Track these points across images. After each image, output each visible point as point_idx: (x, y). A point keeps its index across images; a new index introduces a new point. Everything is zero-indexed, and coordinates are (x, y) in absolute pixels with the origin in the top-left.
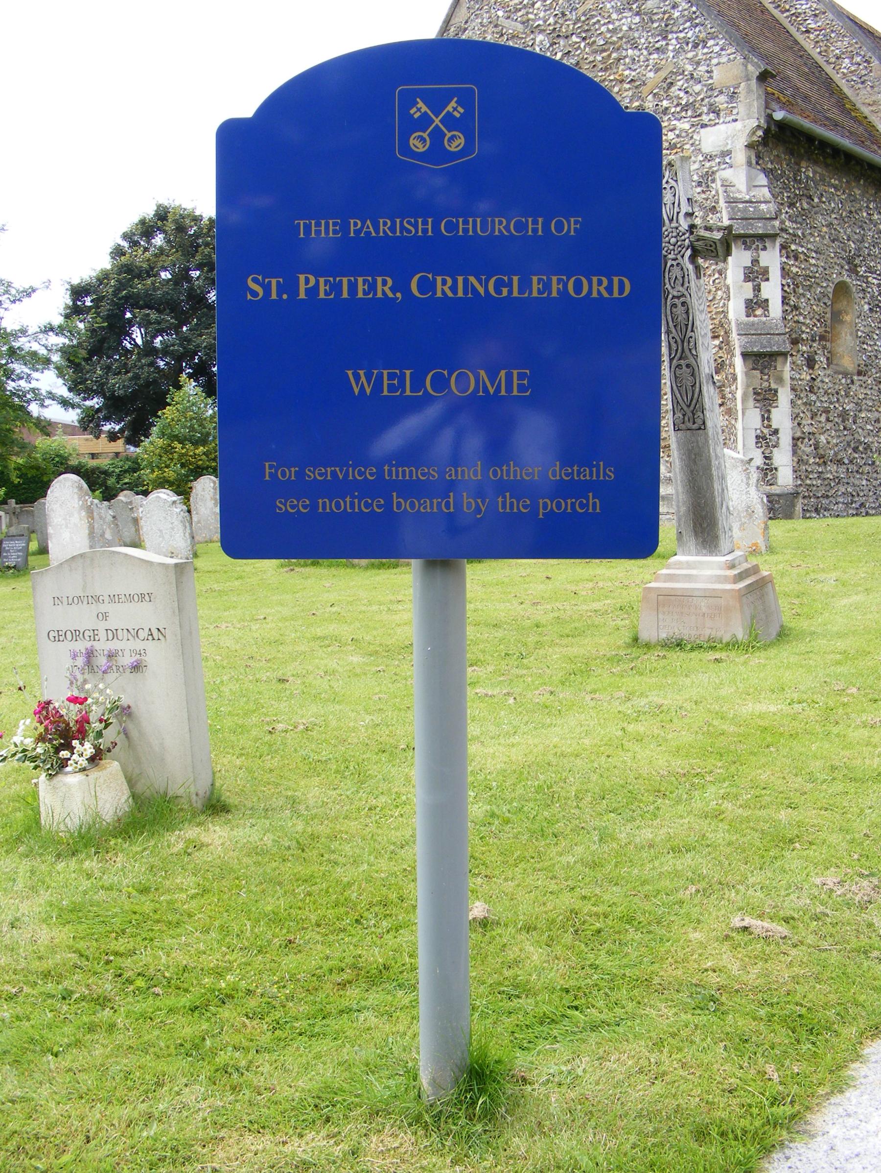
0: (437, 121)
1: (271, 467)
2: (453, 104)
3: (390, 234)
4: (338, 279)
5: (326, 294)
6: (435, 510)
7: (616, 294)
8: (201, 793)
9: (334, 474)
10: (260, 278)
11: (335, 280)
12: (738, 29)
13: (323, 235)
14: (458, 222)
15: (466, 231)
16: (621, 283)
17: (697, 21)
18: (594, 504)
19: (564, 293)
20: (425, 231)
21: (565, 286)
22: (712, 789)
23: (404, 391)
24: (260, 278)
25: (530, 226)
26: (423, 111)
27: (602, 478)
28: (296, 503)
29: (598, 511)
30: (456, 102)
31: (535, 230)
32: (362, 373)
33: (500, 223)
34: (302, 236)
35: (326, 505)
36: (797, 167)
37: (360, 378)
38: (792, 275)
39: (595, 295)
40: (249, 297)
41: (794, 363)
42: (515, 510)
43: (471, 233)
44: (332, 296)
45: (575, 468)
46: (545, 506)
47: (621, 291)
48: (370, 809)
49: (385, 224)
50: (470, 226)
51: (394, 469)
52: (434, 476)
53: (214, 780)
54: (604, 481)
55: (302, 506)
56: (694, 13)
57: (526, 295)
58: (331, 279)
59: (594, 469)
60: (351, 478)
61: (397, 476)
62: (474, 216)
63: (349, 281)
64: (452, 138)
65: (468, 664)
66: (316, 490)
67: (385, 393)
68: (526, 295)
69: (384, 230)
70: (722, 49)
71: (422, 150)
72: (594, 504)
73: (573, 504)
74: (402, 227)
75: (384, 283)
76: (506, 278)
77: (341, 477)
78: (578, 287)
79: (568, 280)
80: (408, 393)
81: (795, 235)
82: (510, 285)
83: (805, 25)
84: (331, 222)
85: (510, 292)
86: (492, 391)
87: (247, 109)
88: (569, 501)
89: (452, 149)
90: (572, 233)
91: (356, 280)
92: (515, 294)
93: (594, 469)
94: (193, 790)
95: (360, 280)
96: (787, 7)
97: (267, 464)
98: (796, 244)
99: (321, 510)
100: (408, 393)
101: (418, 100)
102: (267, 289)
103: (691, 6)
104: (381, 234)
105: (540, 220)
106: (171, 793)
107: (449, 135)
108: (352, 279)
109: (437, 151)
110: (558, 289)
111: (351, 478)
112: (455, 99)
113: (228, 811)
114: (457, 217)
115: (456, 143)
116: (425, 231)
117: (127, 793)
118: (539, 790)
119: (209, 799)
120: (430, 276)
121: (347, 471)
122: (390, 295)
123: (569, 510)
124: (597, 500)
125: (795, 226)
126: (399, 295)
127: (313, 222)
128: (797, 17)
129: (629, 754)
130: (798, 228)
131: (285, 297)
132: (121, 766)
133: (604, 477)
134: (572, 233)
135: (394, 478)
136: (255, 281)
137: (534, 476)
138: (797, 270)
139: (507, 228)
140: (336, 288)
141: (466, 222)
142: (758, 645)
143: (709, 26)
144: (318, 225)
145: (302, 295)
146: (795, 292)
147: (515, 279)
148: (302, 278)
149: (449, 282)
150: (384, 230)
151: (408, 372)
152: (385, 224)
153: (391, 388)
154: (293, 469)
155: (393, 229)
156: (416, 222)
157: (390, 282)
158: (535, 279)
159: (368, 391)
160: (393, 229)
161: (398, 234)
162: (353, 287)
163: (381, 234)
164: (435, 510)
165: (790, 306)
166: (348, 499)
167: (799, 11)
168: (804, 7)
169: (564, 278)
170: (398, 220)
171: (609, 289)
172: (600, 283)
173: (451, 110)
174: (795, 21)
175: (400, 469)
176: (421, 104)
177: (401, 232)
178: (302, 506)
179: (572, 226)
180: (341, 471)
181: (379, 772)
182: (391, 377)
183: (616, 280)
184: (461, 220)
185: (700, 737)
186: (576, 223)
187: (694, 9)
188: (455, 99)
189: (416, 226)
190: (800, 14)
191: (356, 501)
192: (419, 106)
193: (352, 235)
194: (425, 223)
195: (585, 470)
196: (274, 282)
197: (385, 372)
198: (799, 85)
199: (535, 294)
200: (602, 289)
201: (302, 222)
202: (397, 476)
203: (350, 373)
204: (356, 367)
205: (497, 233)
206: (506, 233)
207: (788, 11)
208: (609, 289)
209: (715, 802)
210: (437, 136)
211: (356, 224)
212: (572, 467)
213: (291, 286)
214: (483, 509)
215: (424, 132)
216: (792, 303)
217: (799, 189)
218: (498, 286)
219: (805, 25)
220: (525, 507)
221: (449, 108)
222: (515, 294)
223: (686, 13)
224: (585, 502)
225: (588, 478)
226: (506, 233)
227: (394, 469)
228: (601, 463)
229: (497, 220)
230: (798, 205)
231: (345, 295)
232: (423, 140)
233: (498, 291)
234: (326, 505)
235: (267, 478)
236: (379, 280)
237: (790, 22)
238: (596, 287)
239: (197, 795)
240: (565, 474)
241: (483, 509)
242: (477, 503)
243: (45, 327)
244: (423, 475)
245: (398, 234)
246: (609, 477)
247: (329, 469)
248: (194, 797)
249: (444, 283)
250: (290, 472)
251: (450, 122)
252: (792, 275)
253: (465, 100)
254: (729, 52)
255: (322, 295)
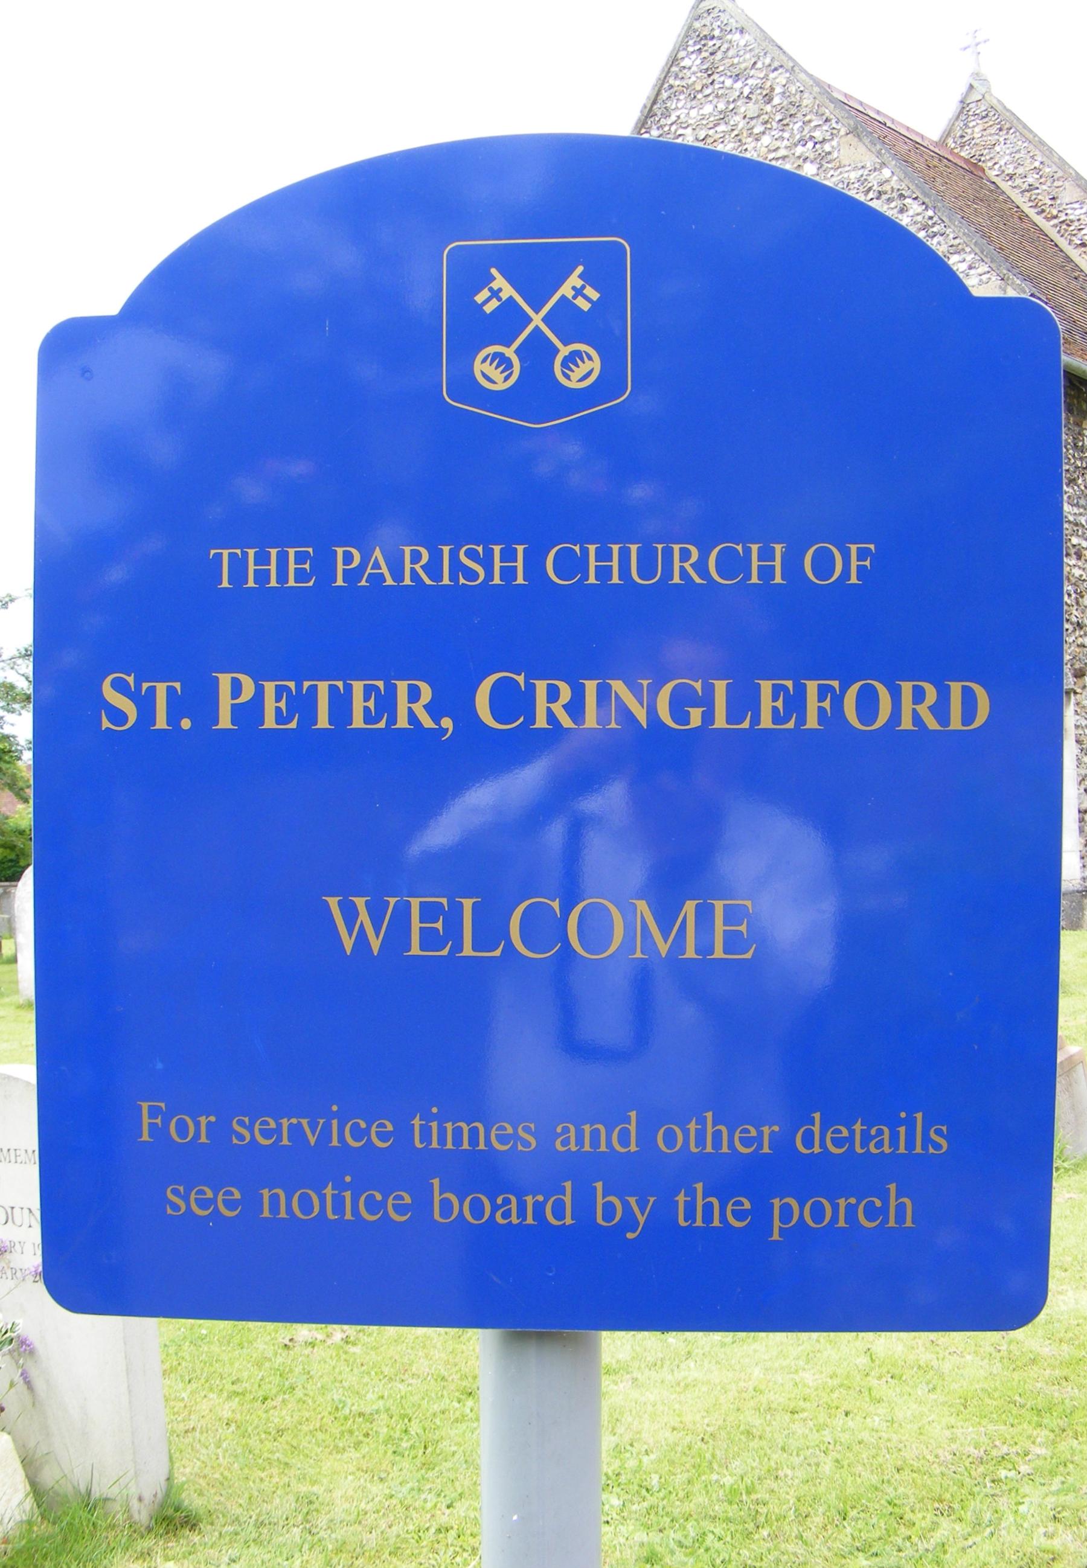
0: (537, 320)
1: (154, 1112)
2: (574, 280)
3: (428, 581)
4: (306, 684)
5: (280, 717)
6: (530, 1220)
7: (956, 723)
8: (148, 1496)
9: (296, 1131)
10: (131, 680)
11: (299, 687)
12: (990, 242)
13: (273, 583)
14: (585, 552)
15: (604, 573)
16: (969, 697)
17: (935, 229)
18: (901, 1208)
19: (834, 718)
20: (508, 574)
21: (838, 702)
22: (1033, 1494)
23: (458, 946)
24: (131, 680)
25: (755, 563)
26: (504, 296)
27: (918, 1150)
28: (210, 1194)
29: (909, 1223)
30: (580, 277)
31: (766, 573)
32: (360, 902)
33: (685, 555)
34: (225, 584)
35: (278, 1203)
36: (1077, 429)
37: (357, 914)
38: (1073, 580)
39: (907, 724)
40: (106, 724)
41: (1078, 704)
42: (716, 1223)
43: (615, 580)
44: (293, 725)
45: (858, 1127)
46: (786, 1211)
47: (969, 713)
48: (439, 1531)
49: (416, 557)
50: (615, 564)
51: (434, 1125)
52: (527, 1144)
53: (171, 1471)
54: (925, 1157)
55: (226, 1201)
56: (931, 218)
57: (746, 725)
58: (292, 685)
59: (902, 1130)
60: (335, 1142)
61: (442, 1140)
62: (625, 538)
63: (333, 689)
64: (573, 359)
65: (603, 1371)
66: (253, 1169)
67: (415, 950)
68: (746, 725)
69: (413, 571)
70: (970, 268)
71: (501, 386)
72: (901, 1208)
73: (851, 1210)
74: (457, 567)
75: (414, 695)
76: (698, 686)
77: (312, 1140)
78: (867, 703)
79: (844, 689)
80: (468, 951)
81: (1076, 524)
82: (707, 701)
83: (1079, 236)
84: (292, 552)
85: (708, 717)
86: (663, 948)
87: (105, 291)
88: (842, 1202)
89: (573, 384)
90: (854, 580)
91: (349, 689)
92: (720, 722)
93: (902, 1130)
94: (133, 1491)
95: (358, 687)
96: (1055, 212)
97: (145, 1106)
98: (1078, 535)
99: (266, 1214)
100: (468, 951)
101: (494, 271)
102: (146, 704)
103: (926, 209)
104: (407, 581)
105: (778, 549)
106: (96, 1494)
107: (564, 351)
108: (340, 684)
109: (537, 386)
110: (821, 711)
111: (335, 1142)
112: (580, 269)
113: (193, 1527)
114: (584, 541)
115: (581, 369)
116: (508, 574)
117: (22, 1486)
118: (732, 1496)
119: (162, 1506)
120: (520, 679)
121: (327, 1127)
122: (427, 722)
123: (842, 1223)
124: (906, 1200)
125: (1076, 510)
126: (447, 723)
127: (251, 552)
128: (1069, 225)
129: (882, 1410)
130: (1081, 514)
131: (186, 724)
132: (14, 1440)
133: (924, 1147)
134: (854, 580)
135: (435, 1145)
136: (120, 686)
137: (760, 1146)
138: (1081, 572)
139: (701, 567)
140: (304, 705)
141: (604, 555)
142: (1065, 1165)
143: (951, 236)
144: (263, 558)
145: (225, 722)
146: (1078, 603)
147: (720, 687)
148: (225, 681)
149: (566, 693)
150: (413, 571)
151: (468, 904)
152: (416, 557)
153: (429, 939)
154: (203, 1120)
155: (434, 569)
156: (489, 553)
157: (426, 693)
158: (766, 687)
159: (375, 944)
160: (434, 569)
161: (446, 581)
162: (341, 704)
163: (407, 581)
164: (530, 1220)
165: (1072, 623)
166: (329, 1191)
167: (1071, 217)
168: (1078, 212)
169: (835, 684)
170: (446, 550)
171: (941, 710)
172: (919, 696)
173: (569, 294)
174: (1066, 230)
175: (449, 1126)
176: (499, 281)
177: (453, 577)
178: (226, 1201)
179: (854, 563)
180: (313, 1126)
181: (459, 1444)
182: (429, 912)
183: (956, 689)
184: (592, 549)
185: (997, 1368)
186: (862, 555)
187: (930, 213)
188: (580, 269)
189: (487, 562)
190: (1072, 221)
191: (348, 1195)
192: (495, 285)
193: (340, 582)
194: (509, 555)
195: (880, 1132)
196: (161, 689)
197: (415, 903)
198: (1076, 316)
199: (766, 722)
200: (923, 710)
201: (225, 553)
202: (442, 1140)
203: (333, 902)
204: (346, 892)
205: (676, 580)
206: (698, 580)
207: (1056, 217)
208: (941, 710)
209: (1042, 1530)
210: (537, 353)
211: (348, 558)
212: (849, 1126)
213: (197, 700)
214: (642, 1219)
215: (508, 346)
216: (1074, 620)
217: (1081, 459)
218: (680, 702)
219: (1079, 236)
220: (739, 1215)
221: (566, 290)
222: (720, 722)
223: (919, 218)
224: (878, 1203)
225: (887, 1149)
226: (698, 580)
227: (434, 1125)
228: (919, 1116)
229: (676, 548)
230: (1080, 481)
231: (323, 721)
232: (504, 362)
233: (681, 716)
234: (278, 1203)
235: (146, 1137)
236: (402, 687)
237: (1059, 232)
238: (910, 706)
239: (140, 1499)
240: (834, 1141)
241: (642, 1219)
242: (626, 1205)
243: (26, 650)
244: (502, 1139)
245: (446, 581)
246: (937, 1146)
247: (285, 1122)
248: (135, 1504)
249: (553, 694)
250: (197, 1125)
251: (567, 321)
252: (1073, 580)
253: (603, 270)
254: (980, 270)
255: (270, 722)
